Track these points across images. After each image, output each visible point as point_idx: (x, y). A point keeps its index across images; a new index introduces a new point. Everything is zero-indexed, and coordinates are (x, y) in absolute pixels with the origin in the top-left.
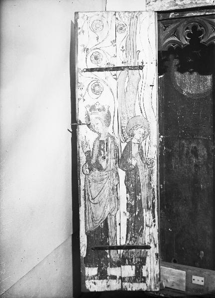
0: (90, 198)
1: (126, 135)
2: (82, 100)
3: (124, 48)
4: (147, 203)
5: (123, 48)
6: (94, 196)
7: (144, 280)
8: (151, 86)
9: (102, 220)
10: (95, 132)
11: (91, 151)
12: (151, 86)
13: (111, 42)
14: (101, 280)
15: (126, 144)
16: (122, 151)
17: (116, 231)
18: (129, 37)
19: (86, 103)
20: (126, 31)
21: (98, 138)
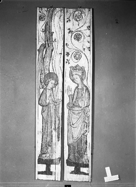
0: (71, 124)
1: (44, 84)
2: (68, 63)
3: (44, 30)
4: (55, 126)
5: (43, 29)
6: (74, 123)
7: (51, 173)
8: (60, 54)
9: (78, 138)
10: (76, 83)
11: (73, 94)
12: (60, 54)
13: (87, 27)
14: (77, 175)
15: (43, 89)
16: (41, 94)
17: (87, 145)
18: (47, 24)
19: (70, 65)
20: (45, 20)
21: (77, 87)
